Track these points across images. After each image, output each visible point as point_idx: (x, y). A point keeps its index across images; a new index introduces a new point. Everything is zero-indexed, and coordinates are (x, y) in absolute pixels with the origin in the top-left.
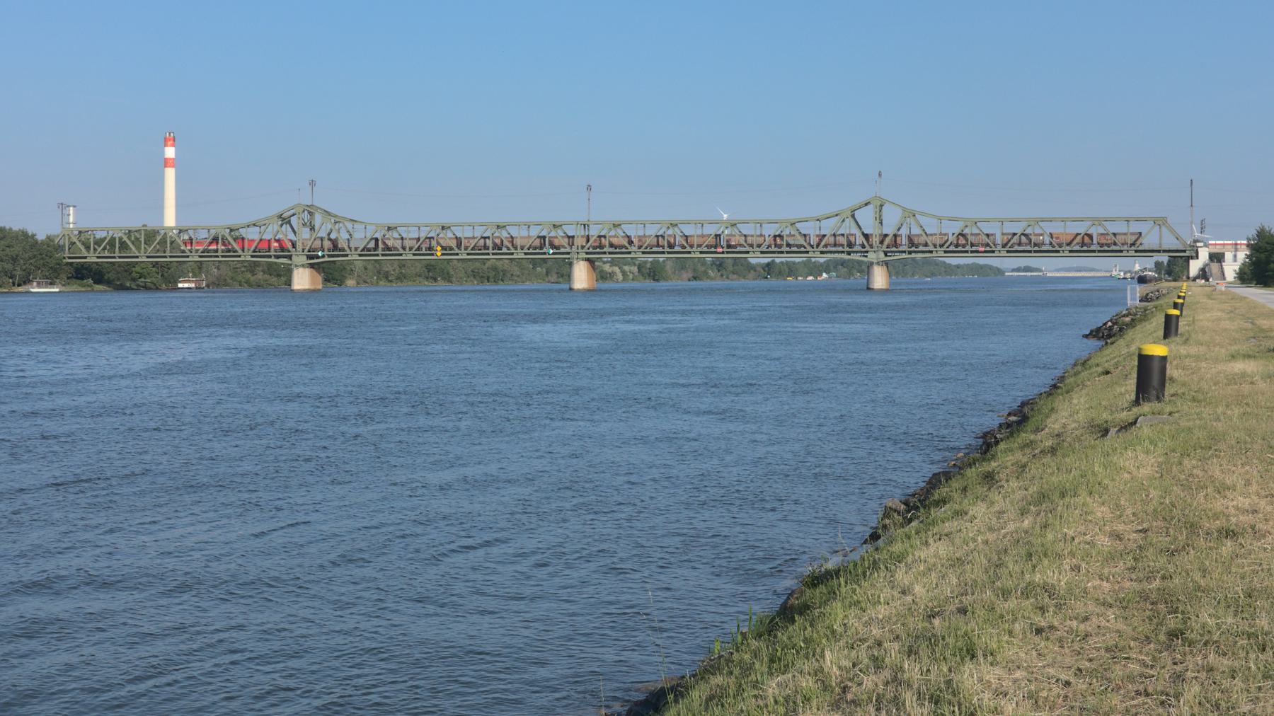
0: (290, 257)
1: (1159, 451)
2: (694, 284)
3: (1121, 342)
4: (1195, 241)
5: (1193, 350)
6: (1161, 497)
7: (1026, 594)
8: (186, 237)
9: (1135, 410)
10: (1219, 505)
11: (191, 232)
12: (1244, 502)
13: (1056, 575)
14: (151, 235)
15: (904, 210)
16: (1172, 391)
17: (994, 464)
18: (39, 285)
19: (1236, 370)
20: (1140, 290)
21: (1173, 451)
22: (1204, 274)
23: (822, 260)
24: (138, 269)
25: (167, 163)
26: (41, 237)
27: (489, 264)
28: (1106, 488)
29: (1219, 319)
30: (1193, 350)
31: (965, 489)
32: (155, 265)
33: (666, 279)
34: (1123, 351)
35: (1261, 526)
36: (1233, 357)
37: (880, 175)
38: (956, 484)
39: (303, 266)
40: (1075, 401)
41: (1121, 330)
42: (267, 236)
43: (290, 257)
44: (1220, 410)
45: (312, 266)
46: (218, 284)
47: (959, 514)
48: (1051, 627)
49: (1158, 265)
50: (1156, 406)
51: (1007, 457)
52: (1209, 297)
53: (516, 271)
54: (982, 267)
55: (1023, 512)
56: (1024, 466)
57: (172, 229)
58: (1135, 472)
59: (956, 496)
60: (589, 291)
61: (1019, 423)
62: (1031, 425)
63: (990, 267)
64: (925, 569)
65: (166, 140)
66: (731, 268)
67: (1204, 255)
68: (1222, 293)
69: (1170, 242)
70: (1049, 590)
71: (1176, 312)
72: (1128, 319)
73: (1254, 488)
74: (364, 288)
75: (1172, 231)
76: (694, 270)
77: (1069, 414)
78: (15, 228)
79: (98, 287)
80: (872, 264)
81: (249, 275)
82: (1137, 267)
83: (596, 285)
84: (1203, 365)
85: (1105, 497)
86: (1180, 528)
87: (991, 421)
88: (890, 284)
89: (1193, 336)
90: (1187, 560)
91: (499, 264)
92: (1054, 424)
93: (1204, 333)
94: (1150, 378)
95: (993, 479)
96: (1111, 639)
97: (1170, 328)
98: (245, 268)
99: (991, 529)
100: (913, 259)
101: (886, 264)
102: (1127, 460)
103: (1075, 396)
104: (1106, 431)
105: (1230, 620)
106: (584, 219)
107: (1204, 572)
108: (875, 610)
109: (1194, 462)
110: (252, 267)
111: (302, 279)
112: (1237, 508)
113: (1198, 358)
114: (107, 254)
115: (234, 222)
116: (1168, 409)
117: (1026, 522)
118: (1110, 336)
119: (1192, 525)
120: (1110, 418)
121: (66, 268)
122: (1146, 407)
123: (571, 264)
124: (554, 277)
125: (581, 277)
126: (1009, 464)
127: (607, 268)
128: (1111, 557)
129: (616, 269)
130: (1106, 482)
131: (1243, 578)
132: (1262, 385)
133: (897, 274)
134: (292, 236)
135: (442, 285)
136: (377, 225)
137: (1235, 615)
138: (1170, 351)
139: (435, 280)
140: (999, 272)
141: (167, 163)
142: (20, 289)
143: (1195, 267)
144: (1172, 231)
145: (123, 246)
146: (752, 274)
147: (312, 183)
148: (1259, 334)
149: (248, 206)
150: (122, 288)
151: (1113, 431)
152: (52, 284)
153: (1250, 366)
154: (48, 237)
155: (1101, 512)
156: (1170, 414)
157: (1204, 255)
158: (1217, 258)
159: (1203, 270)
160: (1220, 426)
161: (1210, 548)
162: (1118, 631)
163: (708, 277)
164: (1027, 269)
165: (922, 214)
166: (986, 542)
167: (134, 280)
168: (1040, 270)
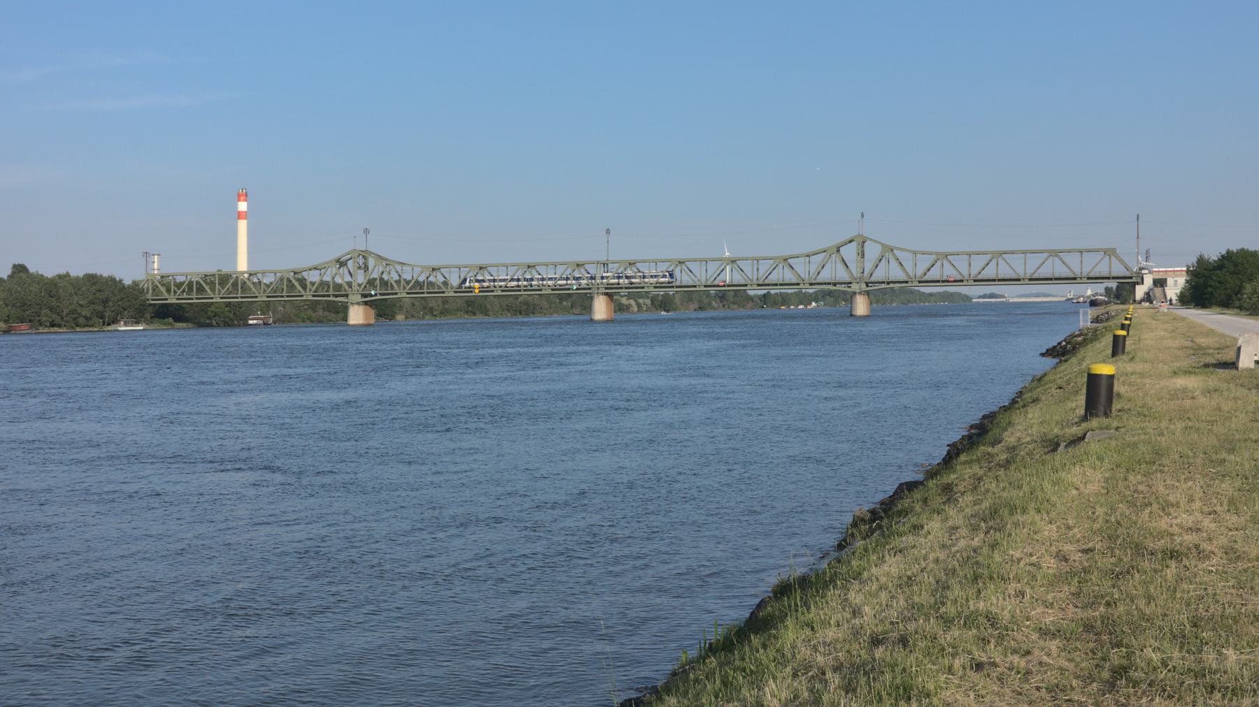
0: (347, 296)
1: (1106, 465)
2: (702, 314)
3: (1074, 360)
4: (1141, 269)
5: (1139, 367)
6: (1106, 514)
7: (970, 621)
8: (256, 280)
9: (1084, 425)
10: (1163, 524)
11: (260, 276)
12: (1186, 519)
13: (998, 602)
14: (224, 279)
15: (883, 245)
16: (1119, 407)
17: (953, 476)
18: (126, 324)
19: (1178, 386)
20: (1091, 312)
21: (1118, 466)
22: (1148, 298)
23: (811, 291)
24: (213, 308)
25: (240, 215)
26: (127, 282)
27: (520, 299)
28: (1054, 505)
29: (1163, 338)
30: (1139, 367)
31: (925, 501)
32: (228, 305)
33: (674, 310)
34: (1074, 369)
35: (1204, 546)
36: (1175, 373)
37: (862, 215)
38: (917, 495)
39: (358, 303)
40: (1030, 416)
41: (1074, 348)
42: (327, 278)
43: (347, 296)
44: (1163, 425)
45: (366, 303)
46: (284, 320)
47: (917, 528)
48: (994, 664)
49: (1108, 290)
50: (1104, 421)
51: (964, 472)
52: (1153, 318)
53: (545, 304)
54: (952, 294)
55: (975, 528)
56: (980, 479)
57: (243, 273)
58: (1082, 487)
59: (918, 508)
60: (369, 325)
61: (979, 435)
62: (990, 436)
63: (959, 294)
64: (879, 589)
65: (239, 195)
66: (732, 299)
67: (1148, 281)
68: (1165, 314)
69: (1119, 270)
70: (992, 620)
71: (1123, 333)
72: (1080, 339)
73: (1198, 505)
74: (412, 321)
75: (1121, 261)
76: (700, 302)
77: (1026, 428)
78: (105, 275)
79: (180, 325)
80: (855, 293)
81: (310, 312)
82: (1089, 293)
83: (613, 316)
84: (1148, 381)
85: (1053, 515)
86: (1130, 551)
87: (955, 436)
88: (872, 310)
89: (1139, 354)
90: (1133, 584)
91: (530, 299)
92: (1010, 438)
93: (1148, 351)
94: (1099, 395)
95: (951, 490)
96: (1052, 677)
97: (1118, 346)
98: (307, 306)
99: (944, 546)
100: (892, 289)
101: (868, 293)
102: (1074, 475)
103: (1030, 410)
104: (1058, 445)
105: (1176, 654)
106: (603, 259)
107: (1150, 599)
108: (820, 634)
109: (1139, 477)
110: (313, 305)
111: (357, 315)
112: (1180, 526)
113: (1142, 375)
114: (185, 296)
115: (296, 266)
116: (1115, 424)
117: (976, 539)
118: (1063, 354)
119: (1137, 545)
120: (1060, 433)
121: (150, 309)
122: (1094, 423)
123: (591, 298)
124: (577, 311)
125: (601, 308)
126: (966, 476)
127: (624, 301)
128: (1055, 581)
129: (632, 302)
130: (1054, 499)
131: (1188, 605)
132: (1202, 400)
133: (877, 302)
134: (348, 278)
135: (480, 318)
136: (422, 267)
137: (1181, 648)
138: (1118, 369)
139: (474, 314)
140: (967, 298)
141: (240, 215)
142: (109, 328)
143: (1140, 291)
144: (1121, 261)
145: (200, 289)
146: (750, 304)
147: (366, 231)
148: (1198, 350)
149: (309, 251)
150: (201, 325)
151: (1063, 444)
152: (137, 323)
153: (1191, 382)
154: (134, 282)
155: (1049, 531)
156: (1117, 429)
157: (1148, 281)
158: (1160, 283)
159: (1148, 294)
160: (1163, 441)
161: (1156, 571)
162: (1061, 668)
163: (712, 308)
164: (992, 296)
165: (898, 249)
166: (937, 561)
167: (209, 318)
168: (1003, 297)
